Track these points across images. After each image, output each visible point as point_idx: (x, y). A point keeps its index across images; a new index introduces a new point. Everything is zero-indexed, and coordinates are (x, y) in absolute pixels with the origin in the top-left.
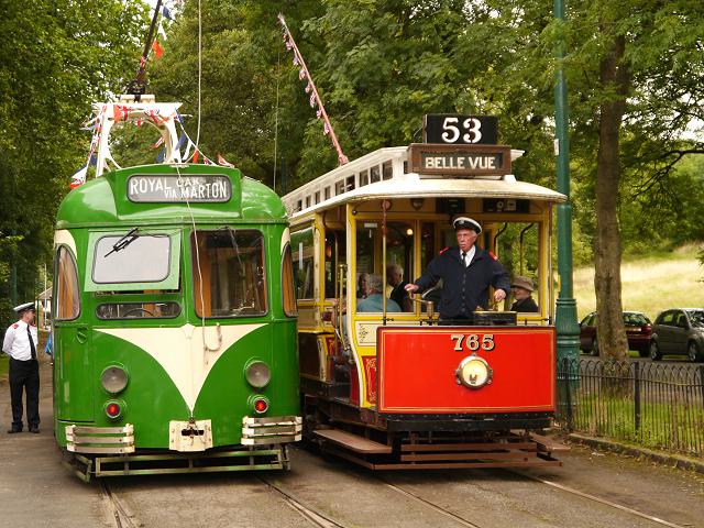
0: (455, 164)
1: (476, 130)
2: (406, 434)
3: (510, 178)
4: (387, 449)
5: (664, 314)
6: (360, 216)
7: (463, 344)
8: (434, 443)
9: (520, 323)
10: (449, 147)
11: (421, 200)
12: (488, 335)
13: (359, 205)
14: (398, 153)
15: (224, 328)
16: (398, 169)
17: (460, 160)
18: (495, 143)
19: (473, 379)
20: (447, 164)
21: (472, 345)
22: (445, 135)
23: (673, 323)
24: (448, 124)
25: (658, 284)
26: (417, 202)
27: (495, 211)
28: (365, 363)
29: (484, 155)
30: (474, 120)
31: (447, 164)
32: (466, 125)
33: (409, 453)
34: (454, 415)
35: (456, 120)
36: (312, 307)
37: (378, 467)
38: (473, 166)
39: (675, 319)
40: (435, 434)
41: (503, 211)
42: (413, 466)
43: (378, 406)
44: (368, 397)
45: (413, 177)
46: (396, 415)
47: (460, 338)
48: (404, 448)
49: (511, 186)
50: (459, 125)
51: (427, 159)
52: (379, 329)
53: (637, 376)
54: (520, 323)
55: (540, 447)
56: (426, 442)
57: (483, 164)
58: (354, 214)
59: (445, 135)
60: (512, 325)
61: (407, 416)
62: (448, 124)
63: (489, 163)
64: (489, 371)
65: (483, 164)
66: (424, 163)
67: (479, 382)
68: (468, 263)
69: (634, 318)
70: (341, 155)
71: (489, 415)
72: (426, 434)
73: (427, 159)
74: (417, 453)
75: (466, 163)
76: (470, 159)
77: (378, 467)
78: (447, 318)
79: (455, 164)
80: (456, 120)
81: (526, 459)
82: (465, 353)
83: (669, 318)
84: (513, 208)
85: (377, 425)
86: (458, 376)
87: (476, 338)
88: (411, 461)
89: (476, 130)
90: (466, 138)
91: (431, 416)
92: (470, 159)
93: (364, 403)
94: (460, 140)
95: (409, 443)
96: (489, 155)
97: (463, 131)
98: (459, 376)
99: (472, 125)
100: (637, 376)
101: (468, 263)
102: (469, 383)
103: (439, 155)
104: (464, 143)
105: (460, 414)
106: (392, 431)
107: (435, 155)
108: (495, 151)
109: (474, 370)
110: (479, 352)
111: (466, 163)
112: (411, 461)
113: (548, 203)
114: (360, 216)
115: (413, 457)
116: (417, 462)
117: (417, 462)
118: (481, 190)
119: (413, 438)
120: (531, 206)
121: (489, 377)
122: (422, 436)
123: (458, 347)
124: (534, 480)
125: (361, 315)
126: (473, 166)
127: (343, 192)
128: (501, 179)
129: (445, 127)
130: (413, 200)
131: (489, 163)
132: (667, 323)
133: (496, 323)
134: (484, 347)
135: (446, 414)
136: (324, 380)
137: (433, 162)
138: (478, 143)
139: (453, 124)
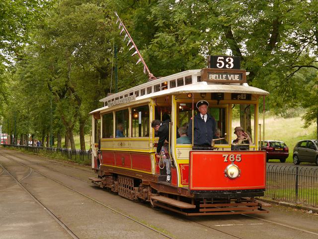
0: (222, 78)
1: (231, 63)
2: (202, 199)
3: (246, 85)
4: (194, 207)
5: (301, 143)
6: (179, 101)
7: (228, 159)
8: (214, 203)
9: (251, 149)
10: (220, 70)
11: (205, 93)
12: (238, 155)
13: (178, 95)
14: (195, 73)
15: (85, 141)
16: (195, 79)
17: (224, 76)
18: (239, 68)
19: (232, 174)
20: (219, 78)
21: (232, 159)
22: (218, 65)
23: (307, 146)
24: (220, 60)
25: (281, 128)
26: (203, 95)
27: (237, 99)
28: (180, 167)
29: (234, 74)
30: (230, 58)
31: (219, 78)
32: (227, 60)
33: (203, 208)
34: (224, 191)
35: (223, 58)
36: (148, 141)
37: (190, 214)
38: (230, 79)
39: (307, 144)
40: (214, 199)
41: (240, 99)
42: (205, 214)
43: (189, 187)
44: (181, 182)
45: (205, 83)
46: (198, 191)
47: (227, 156)
48: (201, 206)
49: (246, 88)
50: (224, 61)
51: (210, 75)
52: (190, 152)
53: (297, 173)
54: (251, 149)
55: (259, 205)
56: (210, 203)
57: (234, 78)
58: (176, 100)
59: (218, 65)
60: (248, 150)
61: (202, 191)
62: (220, 60)
63: (237, 77)
64: (239, 171)
65: (234, 78)
66: (209, 77)
67: (235, 176)
68: (205, 121)
69: (277, 144)
70: (149, 73)
71: (239, 190)
72: (210, 199)
73: (210, 75)
74: (207, 208)
75: (227, 77)
76: (229, 75)
77: (190, 214)
78: (200, 146)
79: (222, 78)
80: (223, 58)
81: (253, 210)
82: (229, 163)
83: (304, 144)
84: (245, 98)
85: (186, 195)
86: (225, 173)
87: (233, 156)
88: (204, 212)
89: (231, 63)
90: (227, 66)
91: (214, 191)
92: (229, 75)
93: (180, 185)
94: (225, 67)
95: (203, 203)
96: (238, 74)
97: (226, 63)
98: (226, 173)
99: (230, 60)
100: (297, 173)
101: (205, 121)
102: (230, 176)
103: (216, 73)
104: (226, 68)
105: (226, 190)
106: (197, 199)
107: (213, 73)
108: (239, 72)
109: (233, 170)
110: (235, 162)
111: (227, 77)
112: (204, 212)
113: (258, 96)
114: (179, 101)
115: (205, 210)
116: (206, 212)
117: (206, 212)
118: (234, 90)
119: (206, 201)
120: (252, 97)
121: (239, 174)
122: (209, 201)
123: (226, 160)
124: (255, 219)
125: (179, 145)
126: (230, 79)
127: (159, 90)
128: (241, 85)
129: (218, 61)
130: (201, 93)
131: (237, 77)
132: (304, 147)
133: (241, 149)
134: (237, 160)
135: (220, 191)
136: (154, 174)
137: (213, 77)
138: (232, 69)
139: (222, 60)
